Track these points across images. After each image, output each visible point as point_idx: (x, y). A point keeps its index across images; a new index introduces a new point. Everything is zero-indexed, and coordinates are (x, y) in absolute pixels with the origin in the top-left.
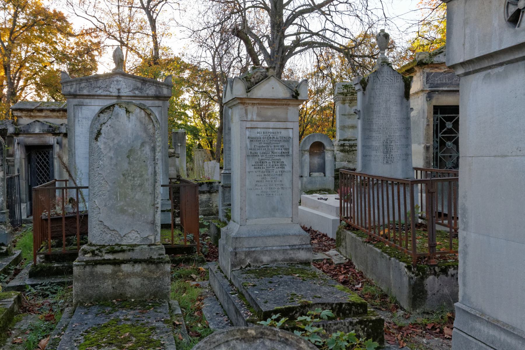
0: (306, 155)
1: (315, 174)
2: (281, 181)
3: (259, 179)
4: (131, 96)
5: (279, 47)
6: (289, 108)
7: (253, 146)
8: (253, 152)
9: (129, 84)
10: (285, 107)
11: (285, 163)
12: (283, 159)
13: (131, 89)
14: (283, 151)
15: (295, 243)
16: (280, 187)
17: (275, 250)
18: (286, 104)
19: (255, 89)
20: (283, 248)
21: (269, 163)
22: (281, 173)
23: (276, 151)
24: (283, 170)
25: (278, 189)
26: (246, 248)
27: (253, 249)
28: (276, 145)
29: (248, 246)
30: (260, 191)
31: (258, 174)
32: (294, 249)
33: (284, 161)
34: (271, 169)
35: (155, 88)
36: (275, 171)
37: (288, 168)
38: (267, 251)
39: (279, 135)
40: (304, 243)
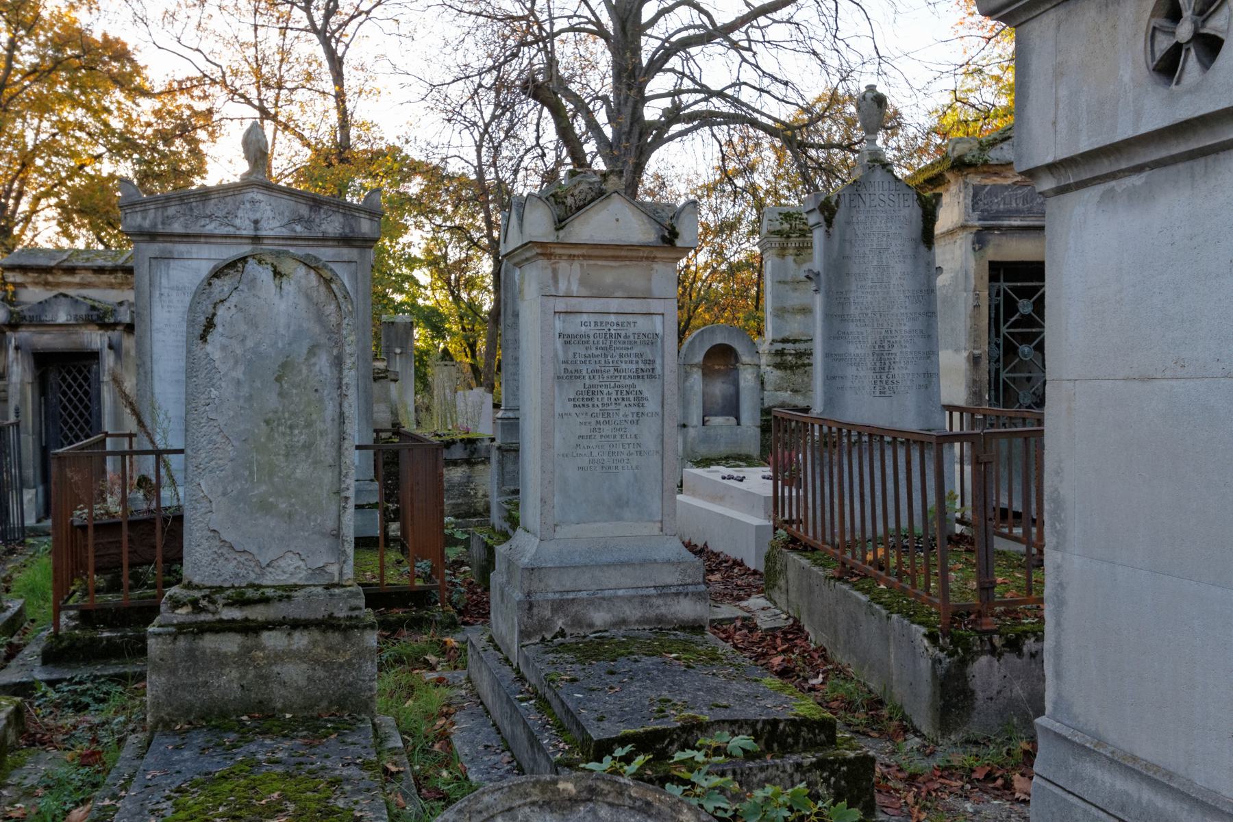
0: (695, 376)
3: (585, 431)
4: (284, 238)
6: (655, 266)
7: (570, 355)
8: (570, 367)
10: (645, 263)
11: (646, 394)
12: (641, 385)
14: (642, 366)
16: (632, 450)
18: (647, 258)
19: (576, 223)
21: (609, 394)
22: (635, 418)
23: (624, 366)
24: (641, 410)
25: (630, 454)
27: (571, 596)
28: (624, 352)
29: (558, 589)
30: (587, 459)
31: (582, 419)
32: (666, 595)
34: (613, 407)
35: (342, 220)
36: (621, 413)
37: (651, 406)
38: (603, 599)
39: (631, 330)
40: (689, 581)
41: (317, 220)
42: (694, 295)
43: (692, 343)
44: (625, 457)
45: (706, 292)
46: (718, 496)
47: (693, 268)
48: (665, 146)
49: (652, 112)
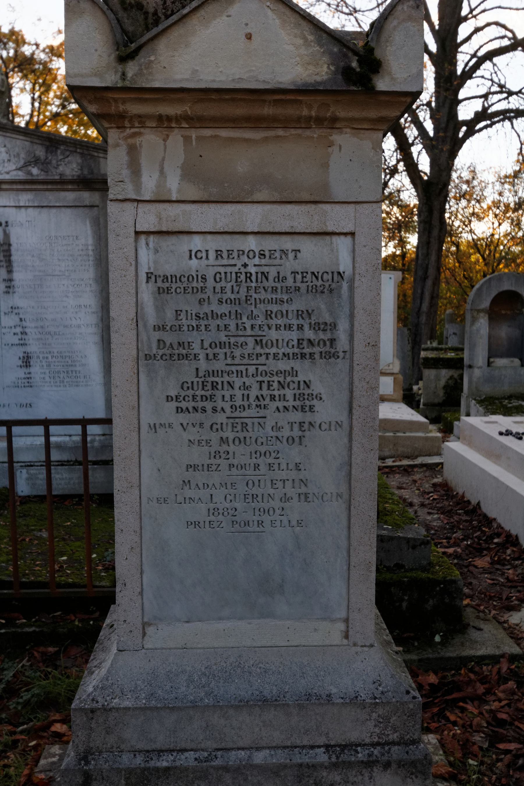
0: (482, 320)
1: (500, 362)
2: (297, 467)
3: (198, 455)
4: (21, 182)
5: (448, 121)
6: (337, 138)
7: (170, 314)
8: (169, 338)
9: (17, 150)
10: (316, 133)
11: (317, 388)
12: (306, 372)
13: (22, 163)
14: (309, 334)
15: (354, 736)
16: (290, 491)
17: (262, 769)
18: (319, 121)
19: (162, 45)
20: (298, 759)
21: (245, 387)
22: (296, 433)
23: (274, 335)
24: (308, 417)
25: (285, 498)
26: (135, 752)
27: (164, 763)
28: (275, 308)
29: (141, 746)
30: (203, 508)
31: (193, 434)
32: (349, 765)
33: (310, 377)
34: (252, 412)
35: (80, 161)
36: (269, 423)
37: (328, 410)
38: (226, 769)
39: (289, 265)
40: (395, 737)
41: (54, 162)
42: (497, 255)
43: (479, 289)
44: (276, 504)
45: (507, 254)
46: (496, 453)
47: (496, 236)
48: (477, 135)
49: (466, 112)
